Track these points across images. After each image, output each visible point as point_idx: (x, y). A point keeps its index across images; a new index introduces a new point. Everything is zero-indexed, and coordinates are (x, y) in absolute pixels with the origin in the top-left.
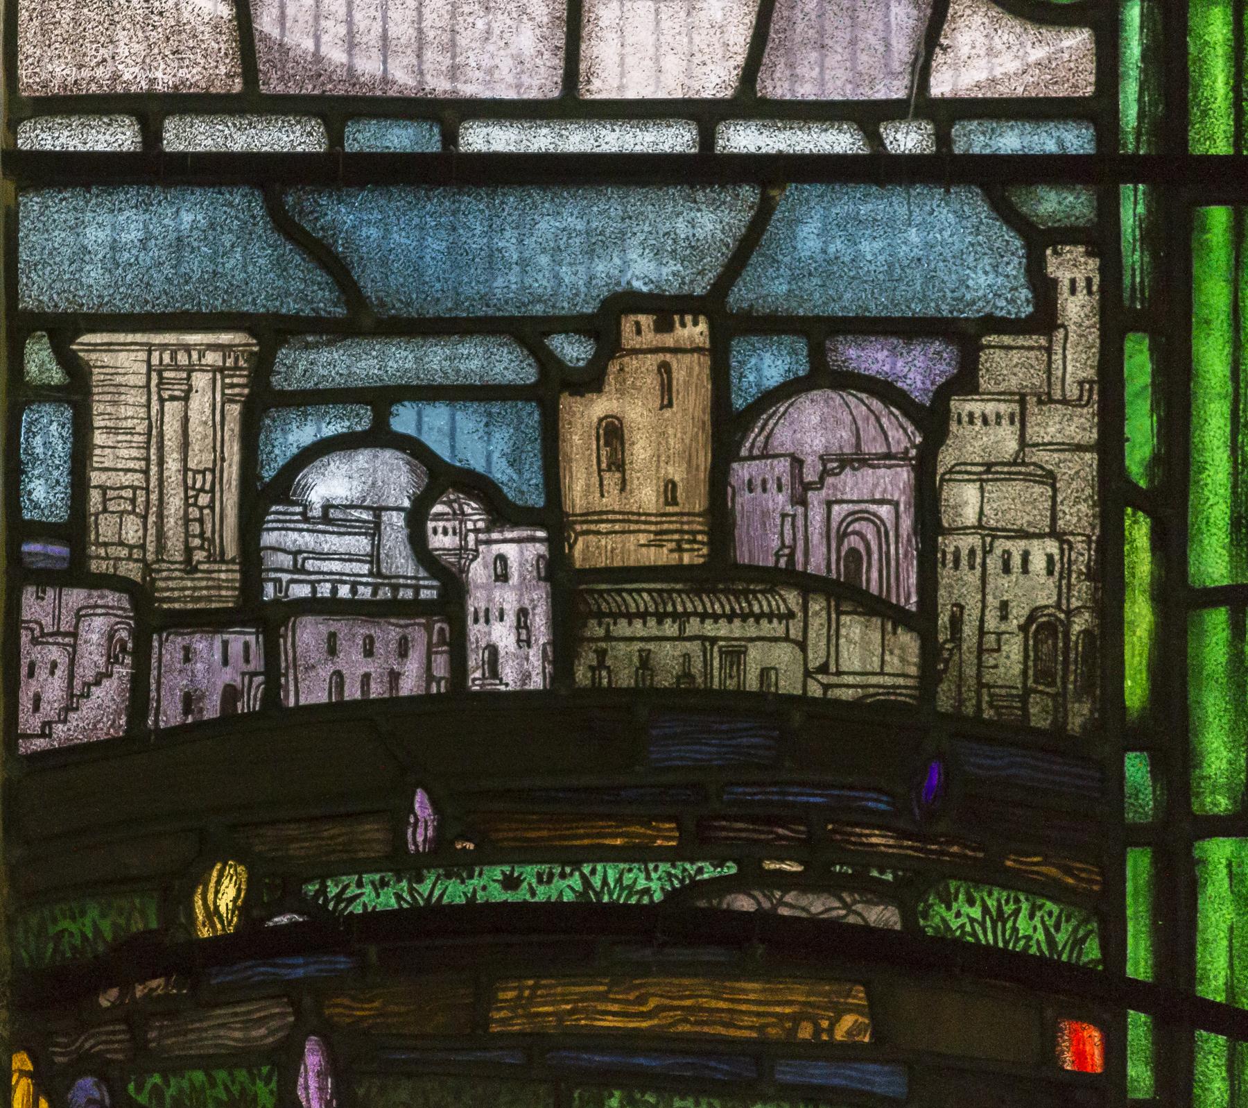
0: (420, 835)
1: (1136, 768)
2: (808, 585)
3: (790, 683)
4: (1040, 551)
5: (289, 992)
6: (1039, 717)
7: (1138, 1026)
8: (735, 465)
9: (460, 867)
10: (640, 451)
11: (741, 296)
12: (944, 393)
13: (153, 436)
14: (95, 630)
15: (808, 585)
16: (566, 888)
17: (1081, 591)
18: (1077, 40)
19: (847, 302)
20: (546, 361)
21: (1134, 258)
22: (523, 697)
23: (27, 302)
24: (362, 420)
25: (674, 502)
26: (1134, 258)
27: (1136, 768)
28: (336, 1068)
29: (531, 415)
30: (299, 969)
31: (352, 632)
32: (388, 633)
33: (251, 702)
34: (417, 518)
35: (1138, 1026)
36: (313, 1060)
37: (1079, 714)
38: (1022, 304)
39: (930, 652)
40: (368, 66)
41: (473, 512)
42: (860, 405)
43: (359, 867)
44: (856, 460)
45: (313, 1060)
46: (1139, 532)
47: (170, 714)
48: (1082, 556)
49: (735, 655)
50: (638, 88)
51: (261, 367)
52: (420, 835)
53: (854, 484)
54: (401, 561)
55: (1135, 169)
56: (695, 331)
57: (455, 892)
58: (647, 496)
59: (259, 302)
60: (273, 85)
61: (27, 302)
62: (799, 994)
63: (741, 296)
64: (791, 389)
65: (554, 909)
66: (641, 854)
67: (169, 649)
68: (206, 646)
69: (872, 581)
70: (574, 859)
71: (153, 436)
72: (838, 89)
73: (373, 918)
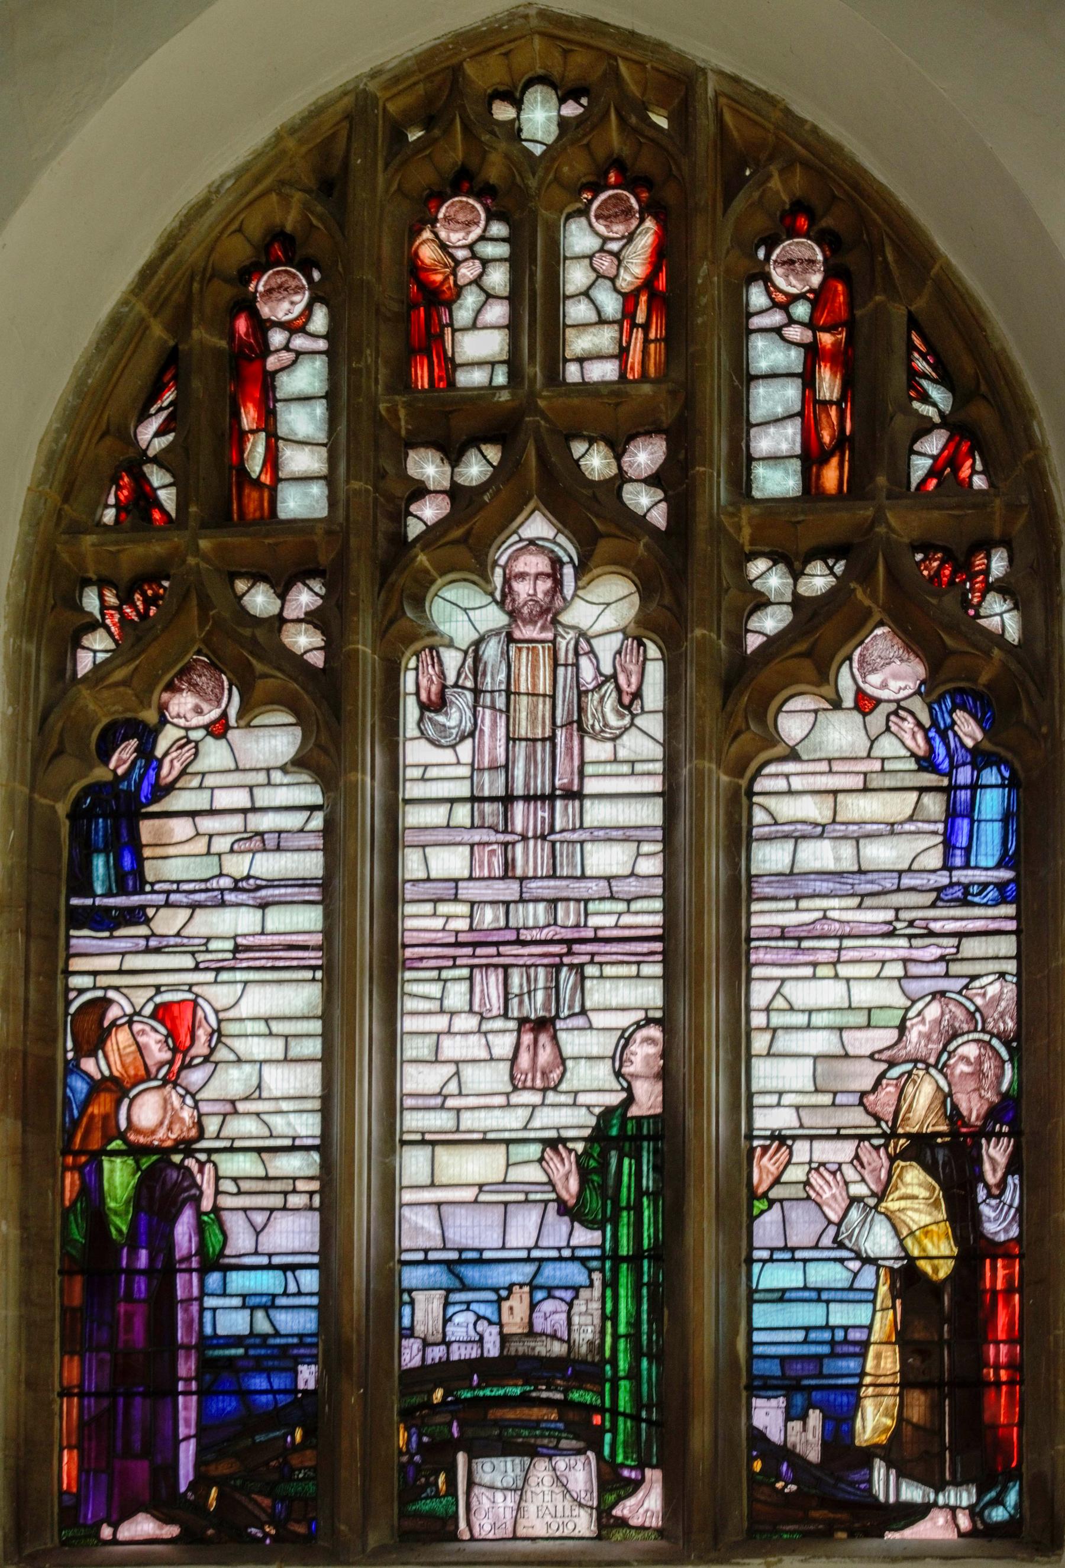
0: (475, 1383)
1: (608, 1368)
2: (547, 1336)
3: (543, 1353)
4: (590, 1329)
5: (451, 1412)
6: (589, 1358)
7: (607, 1416)
8: (300, 585)
9: (483, 1388)
10: (515, 1311)
11: (535, 1282)
12: (572, 1300)
13: (427, 1311)
14: (415, 1347)
15: (547, 1336)
16: (501, 1392)
17: (597, 1336)
18: (598, 1234)
19: (556, 1283)
20: (499, 1296)
21: (608, 1274)
22: (494, 1358)
23: (755, 1372)
24: (464, 1307)
25: (316, 1356)
26: (608, 1274)
27: (608, 1368)
28: (459, 1425)
29: (496, 1306)
30: (452, 1408)
31: (463, 1346)
32: (469, 1346)
33: (444, 1359)
34: (475, 1324)
35: (607, 1416)
36: (455, 1424)
37: (597, 1359)
38: (588, 1283)
39: (569, 1348)
40: (464, 1241)
41: (486, 1323)
42: (557, 1302)
43: (464, 1389)
44: (555, 1312)
45: (455, 1424)
46: (609, 1324)
47: (429, 1362)
48: (598, 1329)
49: (533, 1349)
50: (515, 1245)
51: (446, 1298)
52: (475, 1383)
53: (557, 1317)
54: (472, 1332)
55: (608, 1258)
56: (526, 1289)
57: (481, 1393)
58: (518, 1320)
59: (445, 1285)
60: (448, 1246)
61: (755, 1372)
62: (545, 1411)
63: (535, 1282)
64: (544, 1299)
65: (499, 1397)
66: (516, 1385)
67: (429, 1350)
68: (436, 1349)
69: (559, 1334)
70: (503, 1386)
71: (427, 1311)
72: (551, 1244)
73: (466, 1399)
